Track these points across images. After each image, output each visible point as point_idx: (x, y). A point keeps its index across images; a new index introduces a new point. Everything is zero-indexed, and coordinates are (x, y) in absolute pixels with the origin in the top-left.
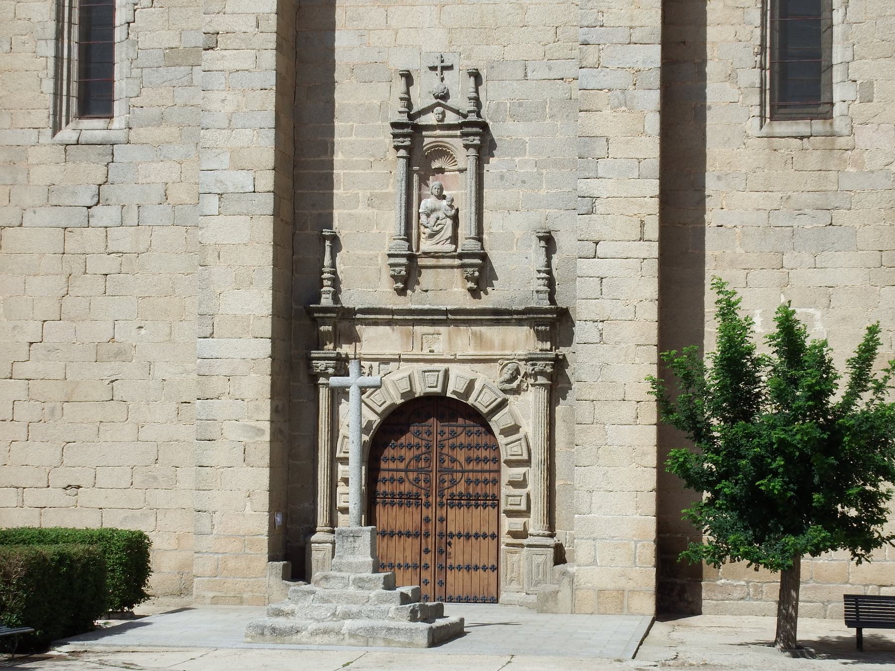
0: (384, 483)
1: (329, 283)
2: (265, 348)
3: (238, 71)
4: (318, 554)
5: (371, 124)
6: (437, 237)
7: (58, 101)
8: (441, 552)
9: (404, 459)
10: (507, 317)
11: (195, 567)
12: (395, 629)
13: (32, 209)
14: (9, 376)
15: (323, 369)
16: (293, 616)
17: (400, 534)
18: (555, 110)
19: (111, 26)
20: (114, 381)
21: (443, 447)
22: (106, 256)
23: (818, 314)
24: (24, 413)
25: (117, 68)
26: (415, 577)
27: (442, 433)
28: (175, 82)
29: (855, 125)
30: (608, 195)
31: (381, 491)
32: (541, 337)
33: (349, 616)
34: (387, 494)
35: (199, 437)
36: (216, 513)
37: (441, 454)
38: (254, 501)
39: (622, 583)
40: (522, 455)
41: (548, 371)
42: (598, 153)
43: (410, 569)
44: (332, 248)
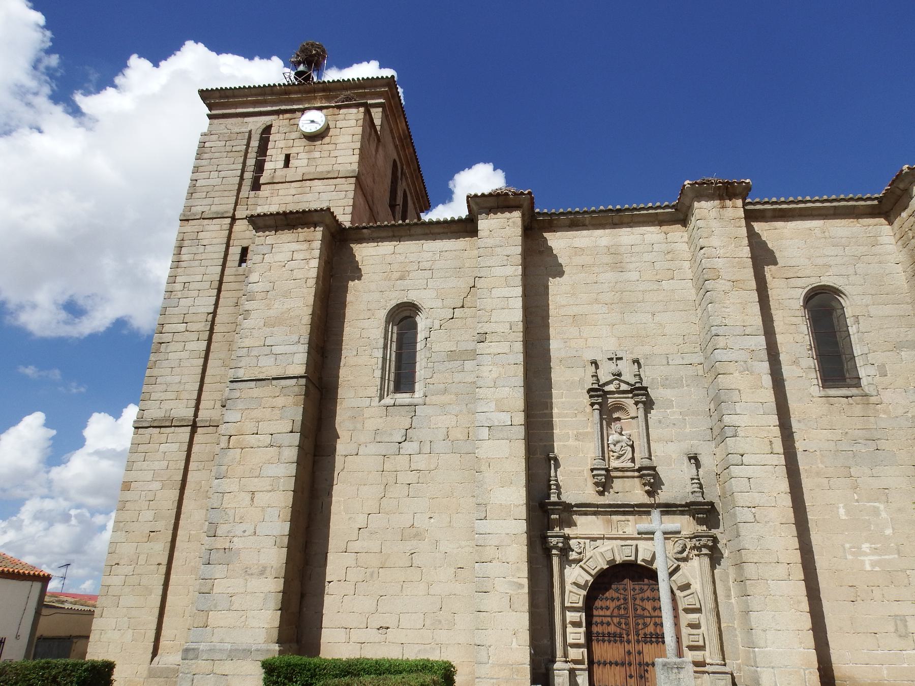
0: (597, 626)
1: (555, 487)
2: (522, 526)
4: (559, 679)
5: (574, 391)
6: (622, 458)
13: (364, 444)
15: (555, 543)
17: (611, 663)
18: (689, 382)
20: (413, 553)
21: (635, 599)
23: (882, 507)
24: (353, 576)
27: (634, 589)
28: (453, 370)
29: (879, 390)
30: (745, 425)
31: (595, 632)
32: (700, 522)
34: (599, 634)
35: (478, 590)
36: (491, 647)
37: (635, 604)
38: (518, 638)
40: (695, 605)
41: (710, 545)
42: (735, 399)
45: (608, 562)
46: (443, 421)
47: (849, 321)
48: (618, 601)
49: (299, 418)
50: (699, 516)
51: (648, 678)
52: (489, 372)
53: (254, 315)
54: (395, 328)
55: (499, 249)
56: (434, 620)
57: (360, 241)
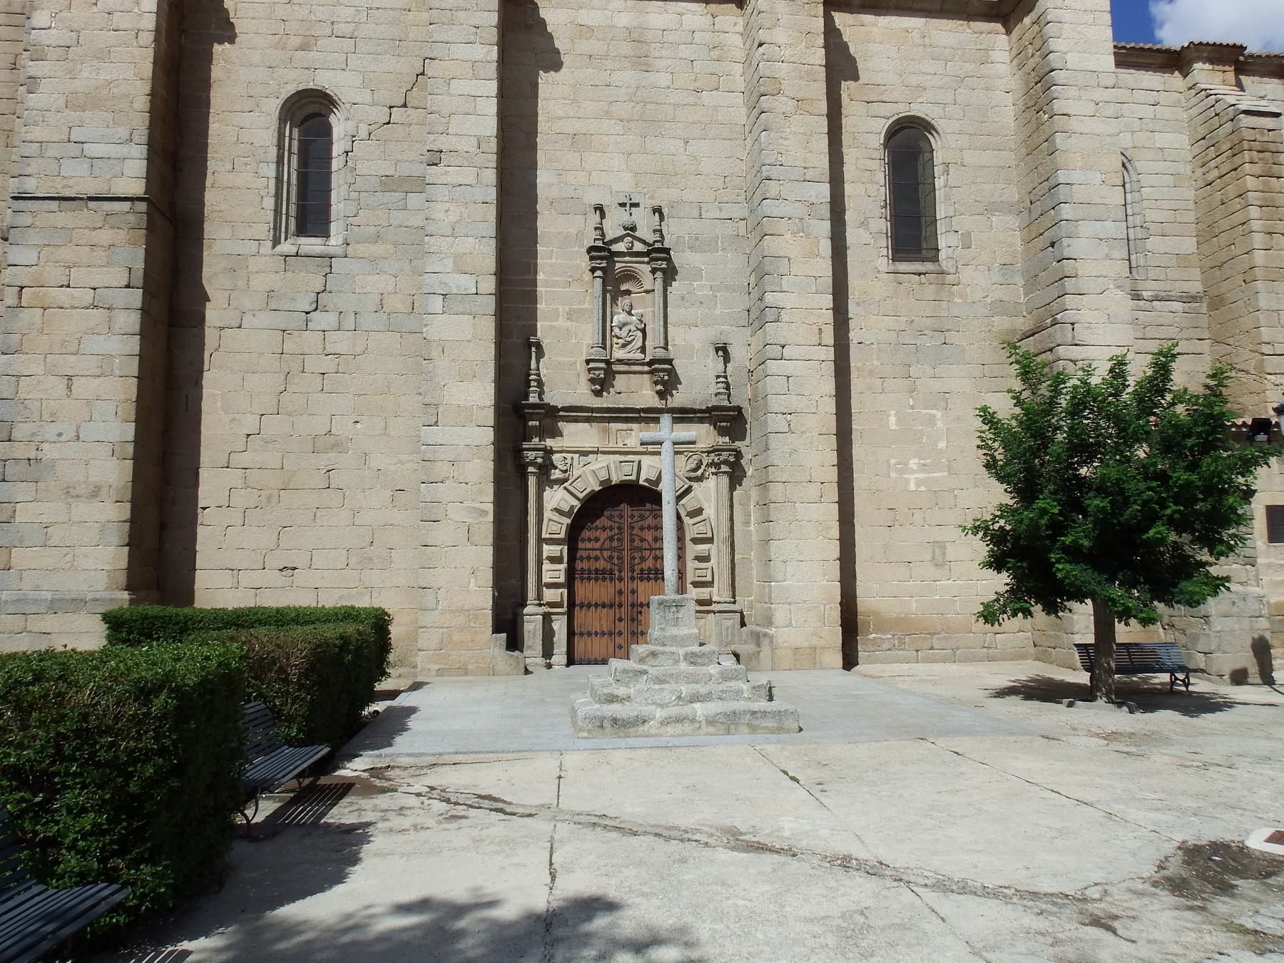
1: (536, 384)
2: (489, 435)
6: (629, 347)
8: (633, 620)
14: (226, 465)
16: (628, 701)
17: (596, 605)
21: (632, 528)
22: (324, 357)
23: (939, 415)
24: (240, 499)
25: (334, 194)
29: (959, 266)
31: (579, 568)
32: (722, 432)
35: (424, 519)
37: (632, 535)
39: (815, 641)
45: (601, 483)
46: (375, 284)
47: (938, 170)
48: (611, 531)
49: (140, 265)
52: (445, 212)
53: (45, 85)
54: (296, 132)
55: (462, 14)
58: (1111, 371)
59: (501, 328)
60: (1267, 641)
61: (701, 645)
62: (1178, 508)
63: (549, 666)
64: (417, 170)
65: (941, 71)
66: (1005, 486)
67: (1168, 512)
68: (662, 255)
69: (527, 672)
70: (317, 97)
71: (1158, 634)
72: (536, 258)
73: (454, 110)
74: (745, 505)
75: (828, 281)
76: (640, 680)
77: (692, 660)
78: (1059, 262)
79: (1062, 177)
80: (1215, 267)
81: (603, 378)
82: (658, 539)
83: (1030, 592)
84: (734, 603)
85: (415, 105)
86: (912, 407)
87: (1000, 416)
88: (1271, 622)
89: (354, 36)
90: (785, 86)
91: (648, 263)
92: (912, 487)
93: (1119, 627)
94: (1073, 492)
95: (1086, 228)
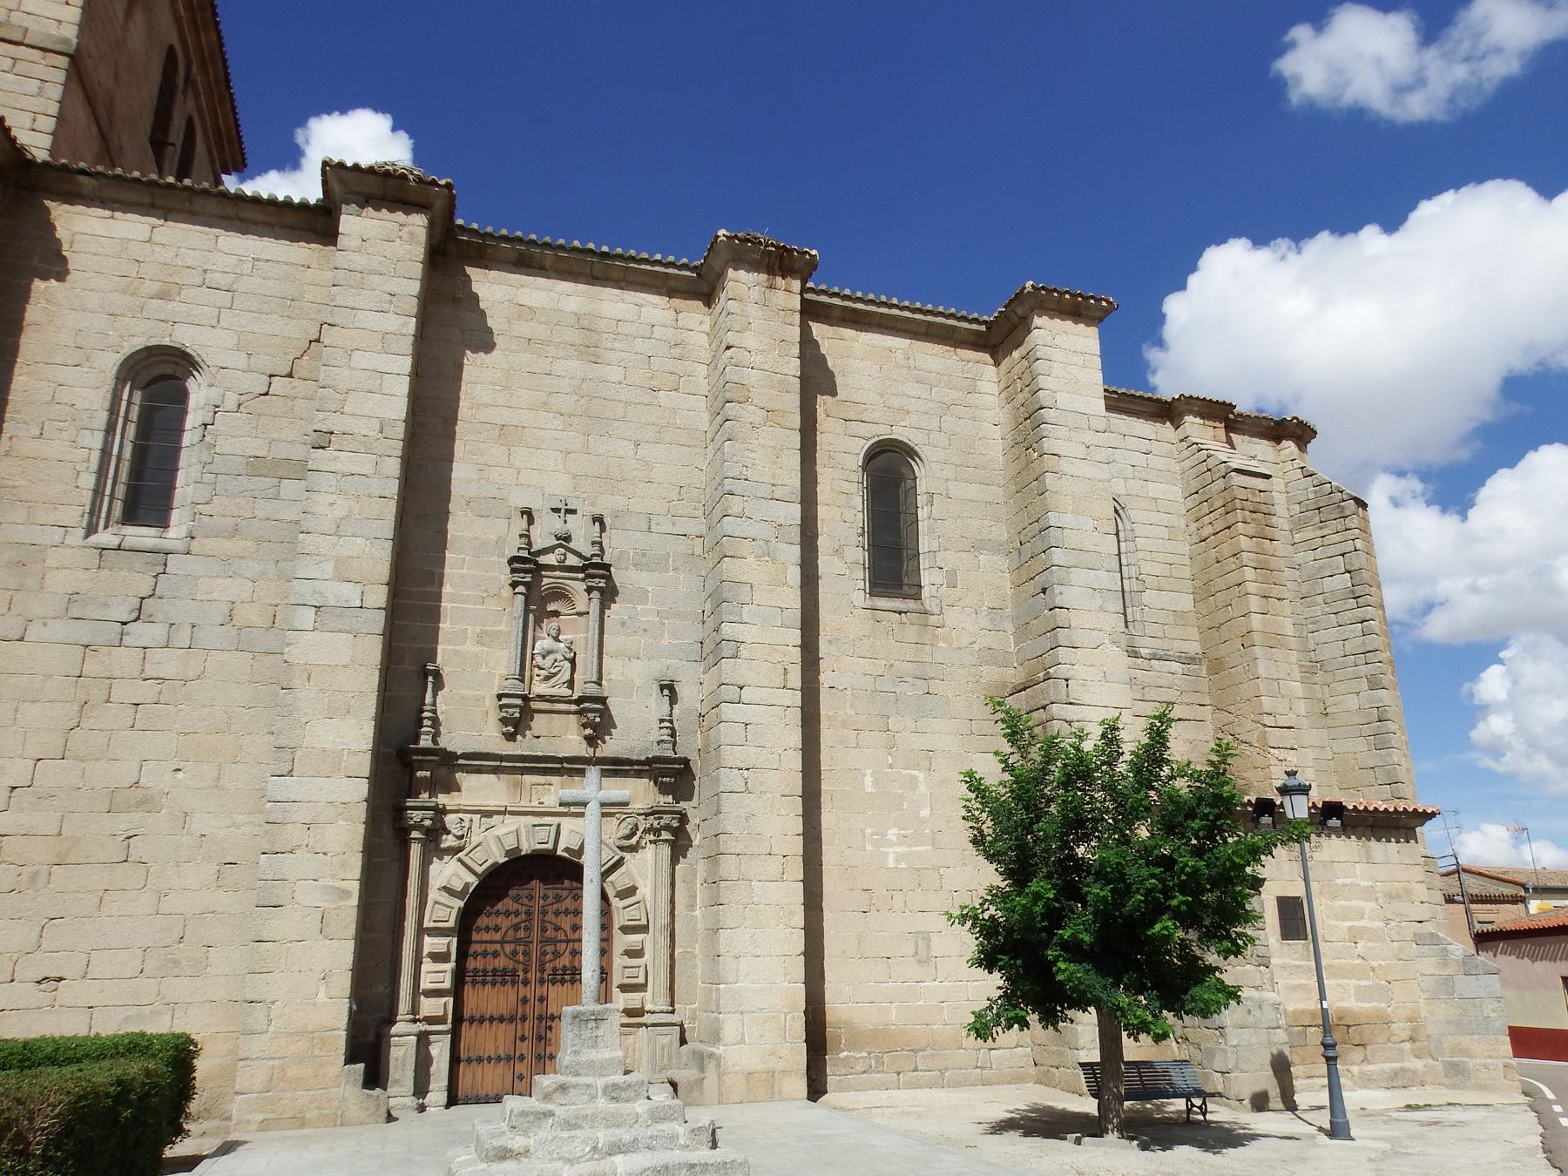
1: (430, 723)
2: (361, 789)
3: (353, 474)
4: (399, 1051)
7: (98, 499)
8: (540, 1038)
9: (500, 928)
10: (627, 768)
11: (238, 1080)
12: (700, 1164)
15: (419, 820)
16: (526, 1157)
17: (492, 1019)
19: (180, 430)
21: (545, 913)
23: (921, 776)
25: (181, 475)
26: (508, 1071)
27: (545, 897)
28: (256, 494)
31: (472, 968)
32: (664, 789)
33: (620, 1149)
34: (498, 971)
35: (261, 903)
37: (544, 921)
38: (330, 984)
41: (675, 825)
43: (502, 1062)
44: (433, 688)
45: (508, 853)
46: (224, 589)
48: (516, 916)
50: (664, 779)
51: (550, 1040)
52: (328, 505)
54: (138, 396)
55: (376, 279)
56: (164, 960)
57: (72, 197)
58: (1103, 736)
59: (390, 652)
60: (1286, 1057)
61: (627, 1072)
62: (1185, 898)
63: (422, 1108)
64: (297, 452)
65: (926, 395)
66: (994, 866)
67: (1174, 902)
68: (601, 572)
69: (390, 1118)
70: (174, 356)
71: (1172, 1050)
72: (443, 567)
73: (353, 386)
74: (690, 883)
75: (797, 614)
76: (543, 1125)
77: (614, 1095)
78: (1051, 610)
79: (1053, 518)
80: (1213, 629)
81: (516, 725)
82: (577, 928)
83: (1027, 999)
84: (673, 1012)
85: (304, 377)
86: (891, 766)
87: (987, 782)
88: (1289, 1034)
89: (233, 289)
90: (754, 393)
91: (583, 580)
92: (891, 864)
93: (1127, 1041)
94: (1070, 874)
95: (1078, 576)
